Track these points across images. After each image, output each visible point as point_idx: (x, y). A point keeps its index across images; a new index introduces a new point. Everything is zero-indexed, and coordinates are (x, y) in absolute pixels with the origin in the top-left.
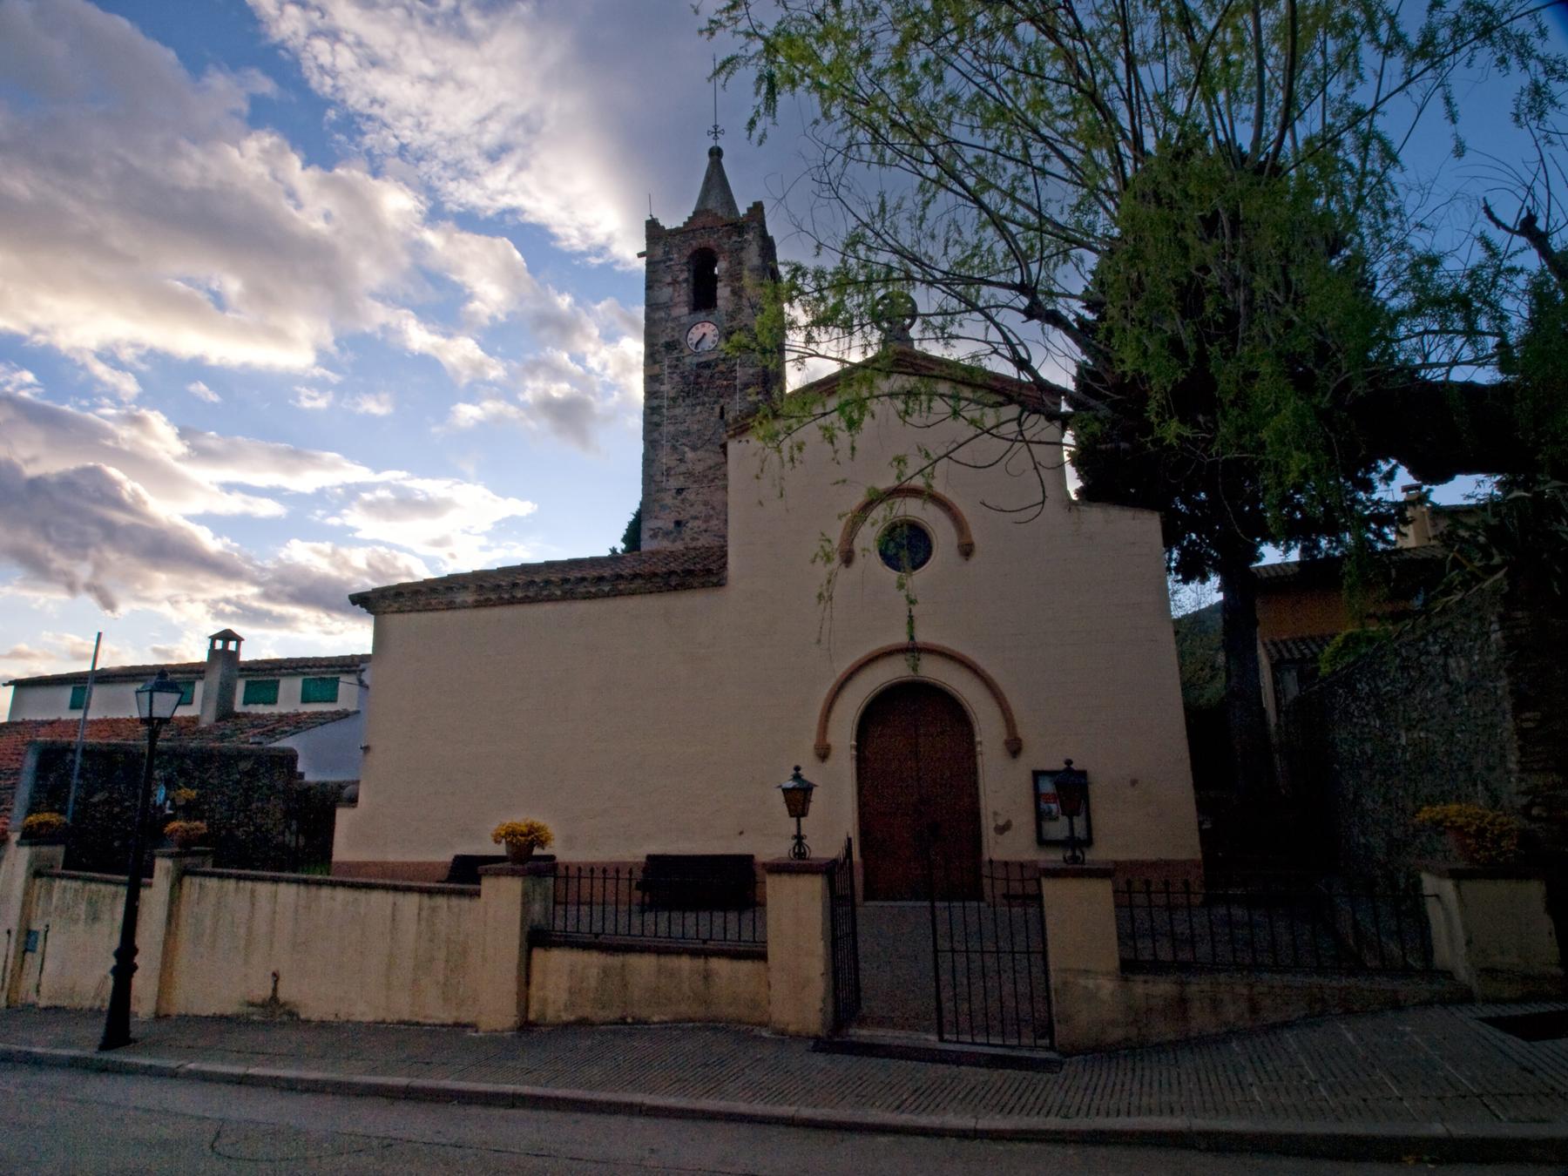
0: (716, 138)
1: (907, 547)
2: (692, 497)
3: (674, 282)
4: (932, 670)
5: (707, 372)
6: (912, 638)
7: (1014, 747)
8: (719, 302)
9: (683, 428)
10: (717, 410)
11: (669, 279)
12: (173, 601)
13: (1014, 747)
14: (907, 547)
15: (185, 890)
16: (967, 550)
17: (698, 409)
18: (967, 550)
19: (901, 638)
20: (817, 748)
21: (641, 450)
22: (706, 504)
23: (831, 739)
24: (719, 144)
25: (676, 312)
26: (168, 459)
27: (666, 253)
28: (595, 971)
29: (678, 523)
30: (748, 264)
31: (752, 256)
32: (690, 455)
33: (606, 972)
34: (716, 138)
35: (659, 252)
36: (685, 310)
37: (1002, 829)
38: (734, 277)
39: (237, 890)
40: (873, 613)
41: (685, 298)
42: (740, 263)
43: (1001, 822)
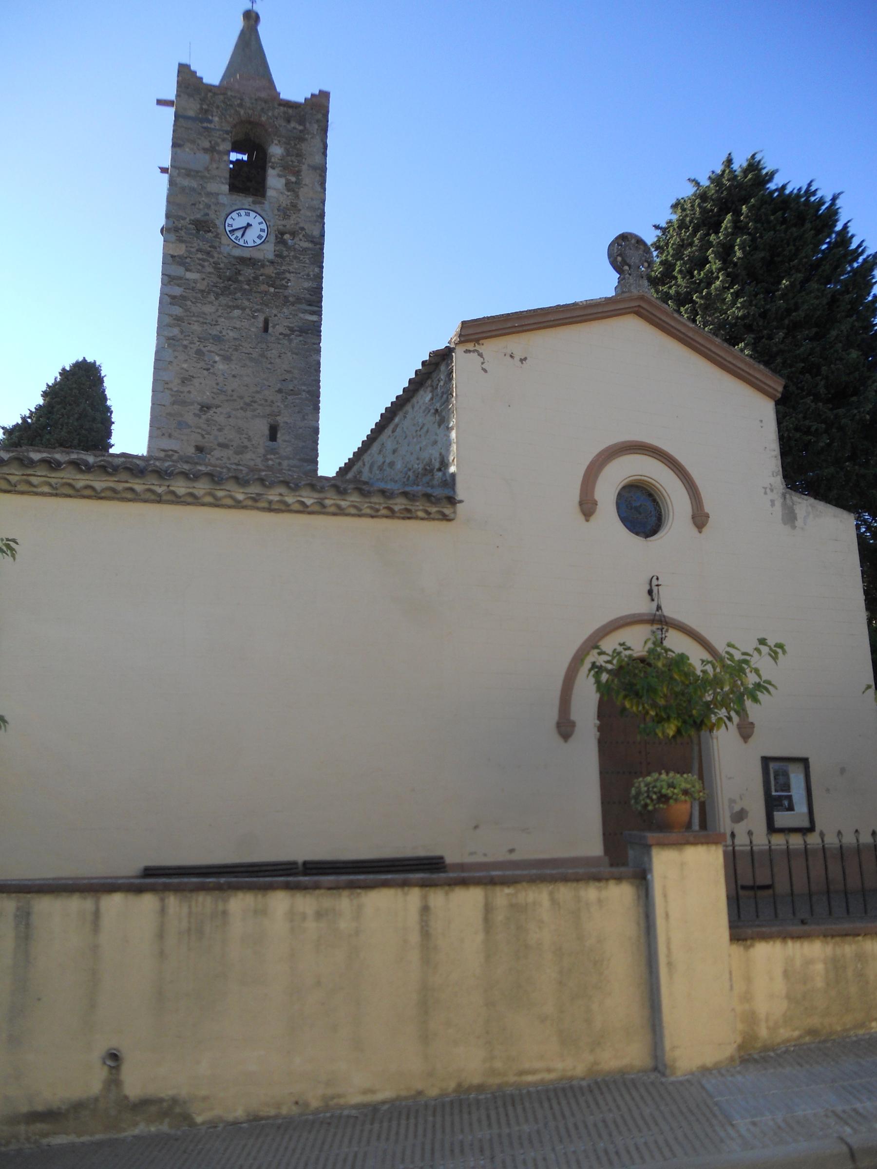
2: (221, 419)
5: (248, 272)
8: (270, 193)
9: (214, 332)
10: (261, 319)
11: (207, 145)
14: (642, 511)
16: (700, 520)
17: (237, 312)
18: (700, 520)
19: (644, 607)
20: (559, 725)
22: (240, 431)
23: (575, 715)
24: (257, 8)
25: (212, 187)
26: (653, 299)
28: (820, 967)
29: (200, 449)
32: (221, 366)
33: (836, 966)
35: (192, 108)
36: (225, 188)
37: (739, 816)
39: (554, 901)
40: (601, 580)
43: (737, 808)
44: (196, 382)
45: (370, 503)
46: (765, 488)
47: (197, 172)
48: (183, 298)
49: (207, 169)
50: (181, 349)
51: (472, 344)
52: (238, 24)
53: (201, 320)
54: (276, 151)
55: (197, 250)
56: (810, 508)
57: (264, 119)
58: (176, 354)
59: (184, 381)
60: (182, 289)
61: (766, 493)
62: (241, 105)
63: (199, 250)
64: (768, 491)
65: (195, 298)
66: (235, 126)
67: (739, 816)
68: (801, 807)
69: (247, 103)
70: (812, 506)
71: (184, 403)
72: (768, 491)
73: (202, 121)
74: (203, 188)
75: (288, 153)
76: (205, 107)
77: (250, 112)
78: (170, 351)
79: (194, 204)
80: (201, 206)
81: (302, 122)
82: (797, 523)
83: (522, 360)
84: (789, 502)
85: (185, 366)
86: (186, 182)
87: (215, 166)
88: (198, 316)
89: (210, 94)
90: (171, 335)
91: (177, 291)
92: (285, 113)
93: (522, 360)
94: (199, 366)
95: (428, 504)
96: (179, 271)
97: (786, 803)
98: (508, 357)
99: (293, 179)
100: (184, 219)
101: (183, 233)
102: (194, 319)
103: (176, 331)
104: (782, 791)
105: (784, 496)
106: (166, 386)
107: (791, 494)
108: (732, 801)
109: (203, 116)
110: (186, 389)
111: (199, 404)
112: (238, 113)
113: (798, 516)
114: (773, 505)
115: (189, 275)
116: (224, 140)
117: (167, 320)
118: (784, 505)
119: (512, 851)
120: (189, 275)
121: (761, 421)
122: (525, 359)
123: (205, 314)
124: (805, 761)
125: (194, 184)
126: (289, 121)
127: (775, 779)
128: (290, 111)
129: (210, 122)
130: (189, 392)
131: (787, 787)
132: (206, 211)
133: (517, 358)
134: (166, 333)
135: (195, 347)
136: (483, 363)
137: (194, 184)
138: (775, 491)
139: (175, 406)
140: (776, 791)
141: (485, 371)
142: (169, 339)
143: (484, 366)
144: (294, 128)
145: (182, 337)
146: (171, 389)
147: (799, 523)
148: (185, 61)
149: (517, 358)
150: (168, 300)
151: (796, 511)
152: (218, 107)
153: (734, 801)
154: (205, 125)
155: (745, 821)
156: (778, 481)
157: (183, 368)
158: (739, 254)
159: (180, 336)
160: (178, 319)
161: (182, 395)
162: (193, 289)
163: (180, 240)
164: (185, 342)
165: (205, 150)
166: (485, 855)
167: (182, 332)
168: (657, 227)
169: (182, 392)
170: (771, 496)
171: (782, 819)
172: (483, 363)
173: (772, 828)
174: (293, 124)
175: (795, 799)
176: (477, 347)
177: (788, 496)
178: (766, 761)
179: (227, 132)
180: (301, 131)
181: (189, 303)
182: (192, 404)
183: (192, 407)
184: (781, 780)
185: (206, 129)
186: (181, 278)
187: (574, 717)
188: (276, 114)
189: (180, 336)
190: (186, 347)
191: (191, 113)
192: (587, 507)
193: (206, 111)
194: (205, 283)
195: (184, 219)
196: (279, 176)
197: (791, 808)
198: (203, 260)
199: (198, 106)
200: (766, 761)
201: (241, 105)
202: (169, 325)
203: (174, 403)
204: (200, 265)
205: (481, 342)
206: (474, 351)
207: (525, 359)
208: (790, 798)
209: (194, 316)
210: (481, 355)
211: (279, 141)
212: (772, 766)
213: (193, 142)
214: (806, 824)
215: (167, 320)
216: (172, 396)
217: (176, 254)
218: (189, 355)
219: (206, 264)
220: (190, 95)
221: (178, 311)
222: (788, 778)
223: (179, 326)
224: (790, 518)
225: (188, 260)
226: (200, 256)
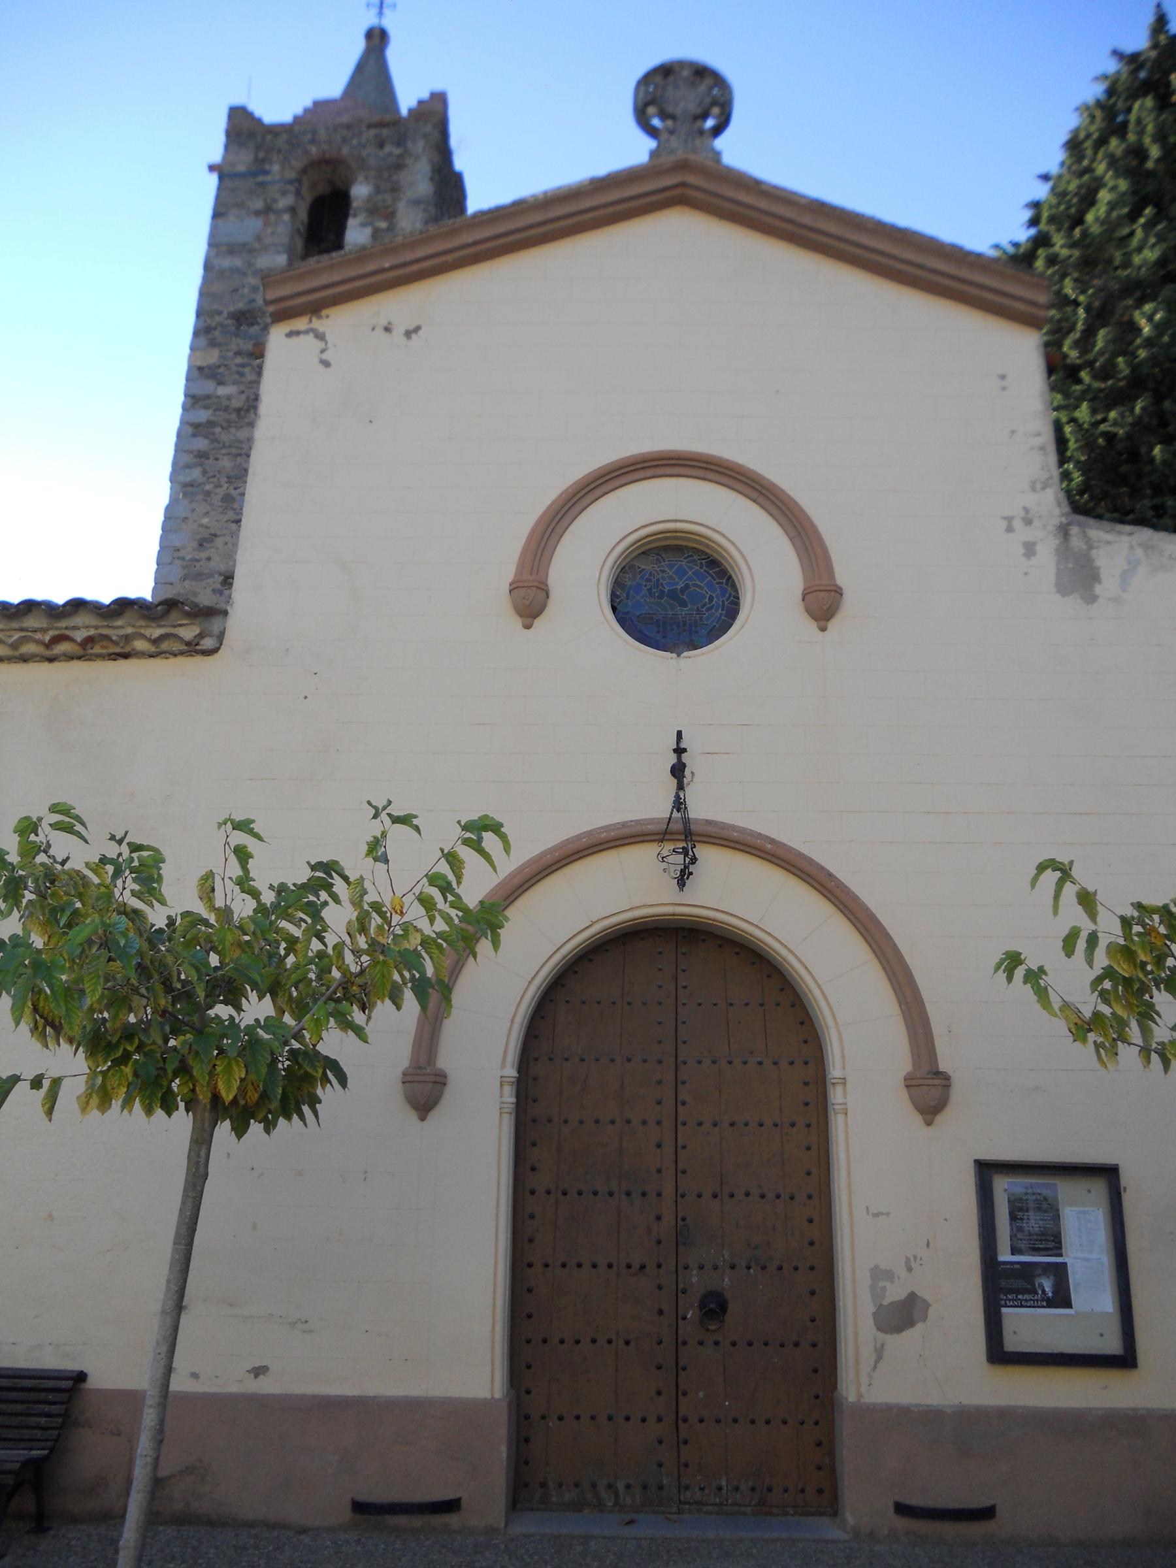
0: (380, 13)
1: (675, 597)
3: (268, 210)
4: (728, 891)
6: (679, 804)
7: (930, 1090)
12: (124, 934)
13: (930, 1090)
14: (675, 597)
15: (1065, 889)
16: (823, 602)
18: (823, 602)
19: (655, 804)
20: (408, 1079)
21: (165, 499)
27: (259, 161)
30: (410, 194)
31: (419, 181)
34: (380, 13)
35: (244, 159)
36: (282, 260)
37: (903, 1315)
38: (381, 211)
41: (285, 240)
42: (395, 189)
43: (895, 1293)
44: (219, 542)
45: (22, 630)
46: (1009, 519)
47: (244, 245)
48: (211, 424)
49: (258, 239)
50: (200, 497)
51: (305, 319)
52: (358, 46)
53: (234, 451)
54: (360, 191)
55: (236, 354)
56: (1139, 552)
57: (345, 151)
58: (194, 505)
59: (202, 544)
60: (210, 412)
61: (1010, 529)
62: (313, 141)
63: (238, 353)
64: (1018, 524)
65: (228, 421)
66: (304, 171)
67: (903, 1315)
68: (1094, 1295)
69: (323, 135)
70: (1147, 547)
71: (199, 576)
72: (1018, 524)
73: (254, 174)
74: (250, 264)
75: (378, 190)
76: (261, 155)
77: (325, 147)
78: (186, 502)
79: (235, 291)
80: (246, 291)
81: (400, 142)
82: (1098, 589)
83: (408, 334)
84: (1076, 542)
85: (205, 521)
86: (226, 263)
87: (269, 231)
88: (230, 447)
89: (269, 137)
90: (188, 479)
91: (203, 416)
92: (376, 136)
93: (408, 334)
94: (226, 518)
95: (142, 623)
96: (208, 387)
97: (1047, 1284)
98: (380, 331)
99: (383, 225)
100: (220, 313)
101: (217, 334)
102: (223, 451)
103: (196, 473)
104: (1035, 1250)
105: (1064, 532)
106: (177, 554)
107: (1081, 525)
108: (880, 1275)
109: (259, 168)
110: (204, 555)
111: (220, 574)
112: (307, 152)
113: (1103, 574)
114: (1030, 549)
115: (222, 391)
116: (284, 193)
117: (187, 458)
118: (1064, 550)
119: (259, 1371)
120: (222, 391)
121: (1003, 377)
122: (417, 329)
123: (241, 442)
124: (1109, 1173)
125: (238, 262)
126: (381, 146)
127: (1013, 1217)
128: (385, 132)
129: (266, 173)
130: (209, 559)
131: (1053, 1241)
132: (253, 296)
133: (399, 331)
134: (181, 478)
135: (221, 492)
136: (322, 351)
137: (238, 262)
138: (1036, 523)
139: (187, 583)
140: (1014, 1251)
141: (326, 364)
142: (185, 485)
143: (324, 356)
144: (390, 154)
145: (204, 480)
146: (183, 559)
147: (1107, 586)
148: (238, 101)
149: (399, 331)
150: (190, 430)
151: (1098, 563)
152: (279, 151)
153: (889, 1276)
154: (260, 179)
155: (919, 1327)
156: (1049, 503)
157: (201, 525)
158: (1155, 152)
159: (202, 479)
160: (202, 456)
161: (198, 565)
162: (226, 409)
163: (213, 344)
164: (208, 487)
165: (258, 213)
166: (195, 1376)
167: (205, 472)
168: (1045, 177)
169: (198, 561)
170: (1023, 533)
171: (1027, 1326)
172: (322, 351)
173: (999, 1354)
174: (388, 148)
175: (1075, 1276)
176: (317, 324)
177: (1074, 530)
178: (987, 1171)
179: (291, 182)
180: (400, 156)
181: (218, 430)
182: (211, 575)
183: (211, 580)
184: (1034, 1222)
185: (262, 185)
186: (208, 397)
187: (445, 1061)
188: (364, 139)
189: (202, 479)
190: (208, 493)
191: (241, 168)
192: (530, 599)
193: (263, 161)
194: (243, 397)
195: (220, 313)
196: (363, 225)
197: (1061, 1299)
198: (243, 366)
199: (252, 156)
200: (987, 1171)
201: (313, 141)
202: (188, 466)
203: (185, 578)
204: (238, 373)
205: (324, 313)
206: (307, 332)
207: (417, 329)
208: (1060, 1272)
209: (224, 447)
210: (320, 337)
211: (366, 178)
212: (1002, 1186)
213: (240, 205)
214: (1112, 1345)
215: (187, 458)
216: (184, 567)
217: (204, 364)
218: (211, 505)
219: (247, 370)
220: (241, 144)
221: (201, 444)
222: (1057, 1218)
223: (201, 464)
224: (1080, 577)
225: (222, 370)
226: (239, 360)
